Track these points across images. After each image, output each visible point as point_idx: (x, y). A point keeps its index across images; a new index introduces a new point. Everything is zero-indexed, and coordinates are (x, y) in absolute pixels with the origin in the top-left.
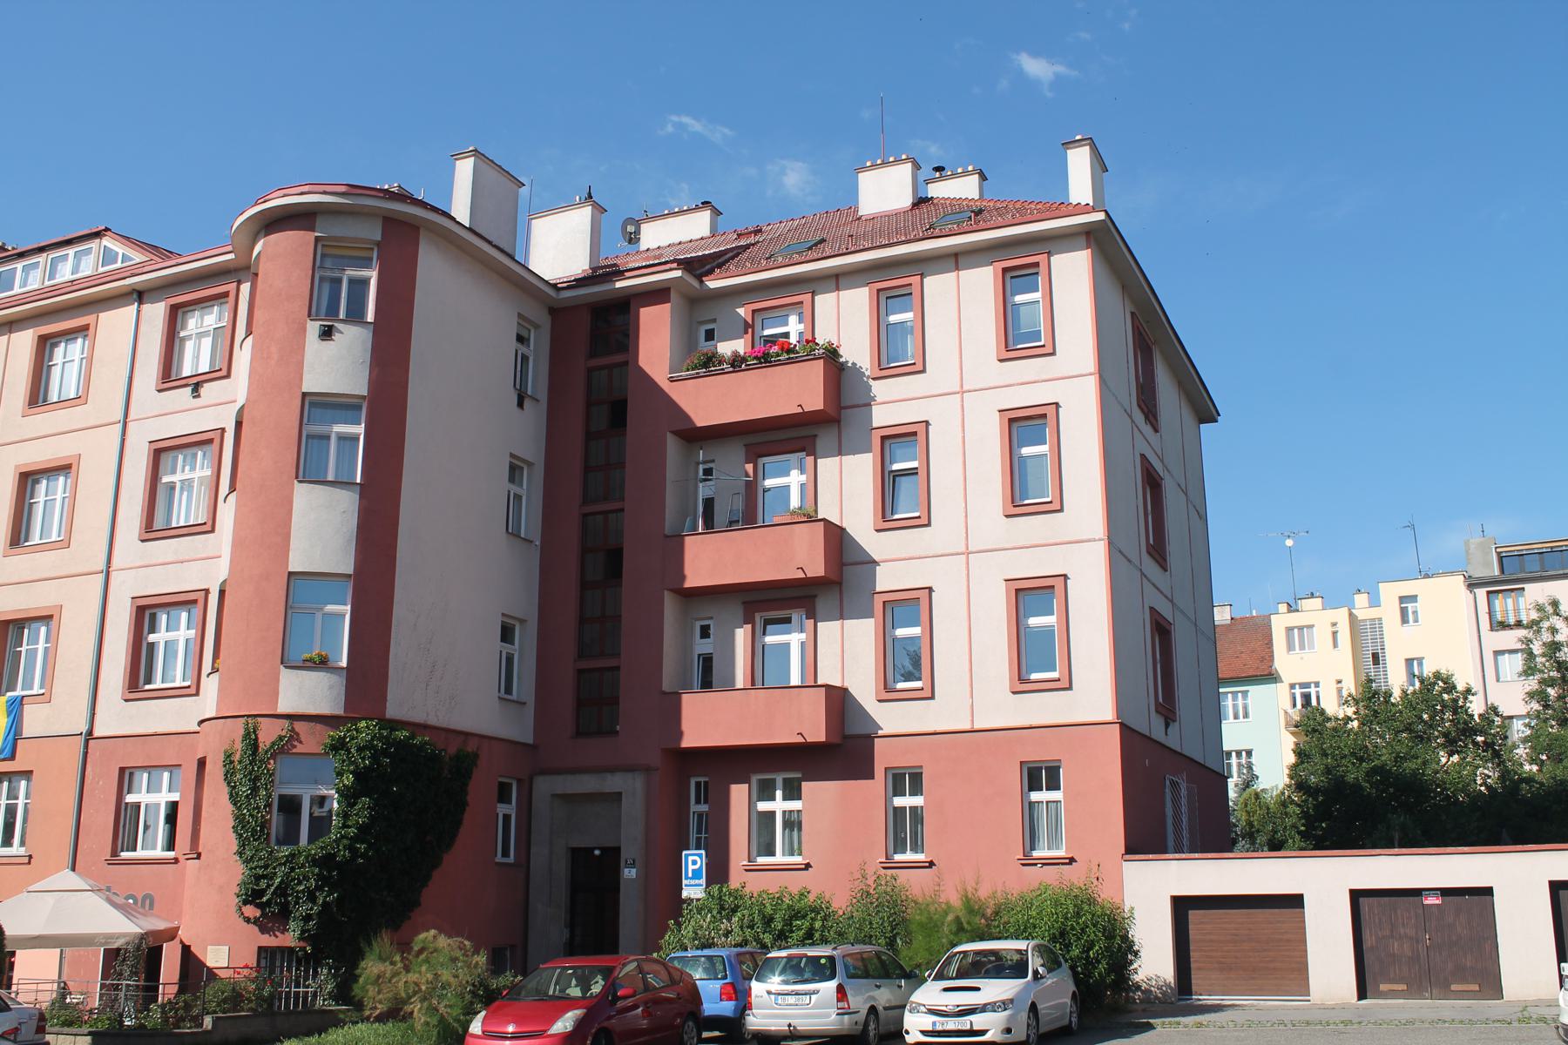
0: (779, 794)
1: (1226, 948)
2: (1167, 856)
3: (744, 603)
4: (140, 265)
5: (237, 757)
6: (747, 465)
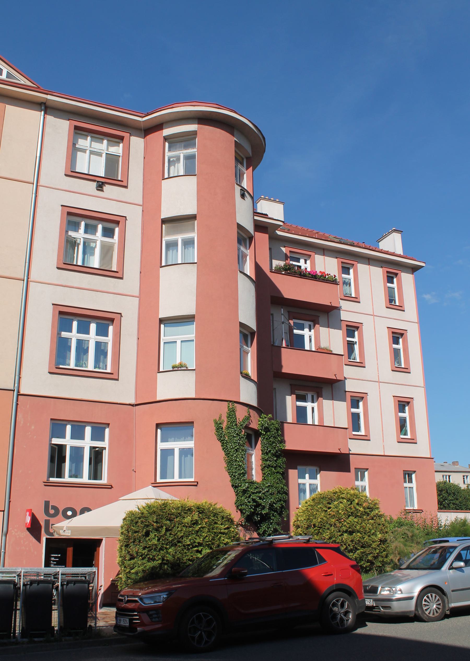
0: (307, 476)
1: (81, 569)
2: (450, 511)
3: (291, 385)
4: (162, 109)
5: (224, 426)
6: (290, 321)
